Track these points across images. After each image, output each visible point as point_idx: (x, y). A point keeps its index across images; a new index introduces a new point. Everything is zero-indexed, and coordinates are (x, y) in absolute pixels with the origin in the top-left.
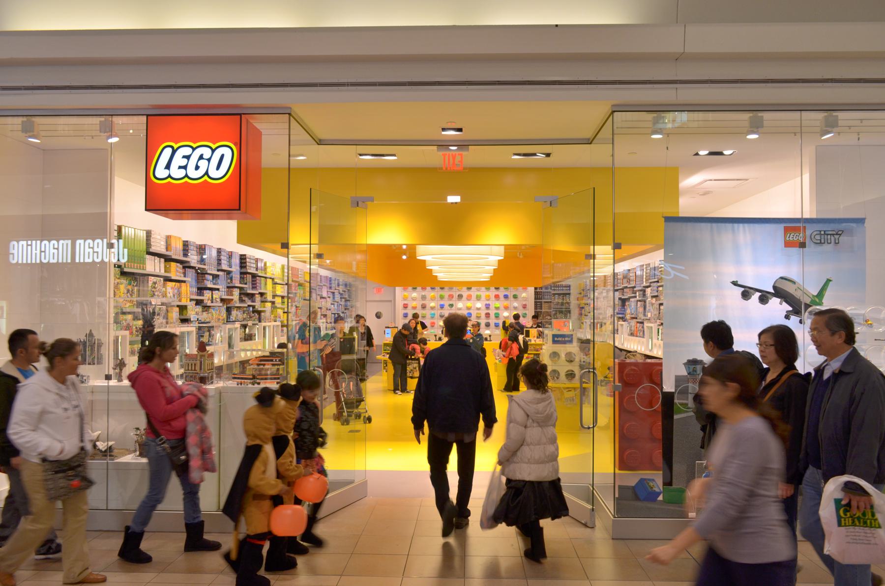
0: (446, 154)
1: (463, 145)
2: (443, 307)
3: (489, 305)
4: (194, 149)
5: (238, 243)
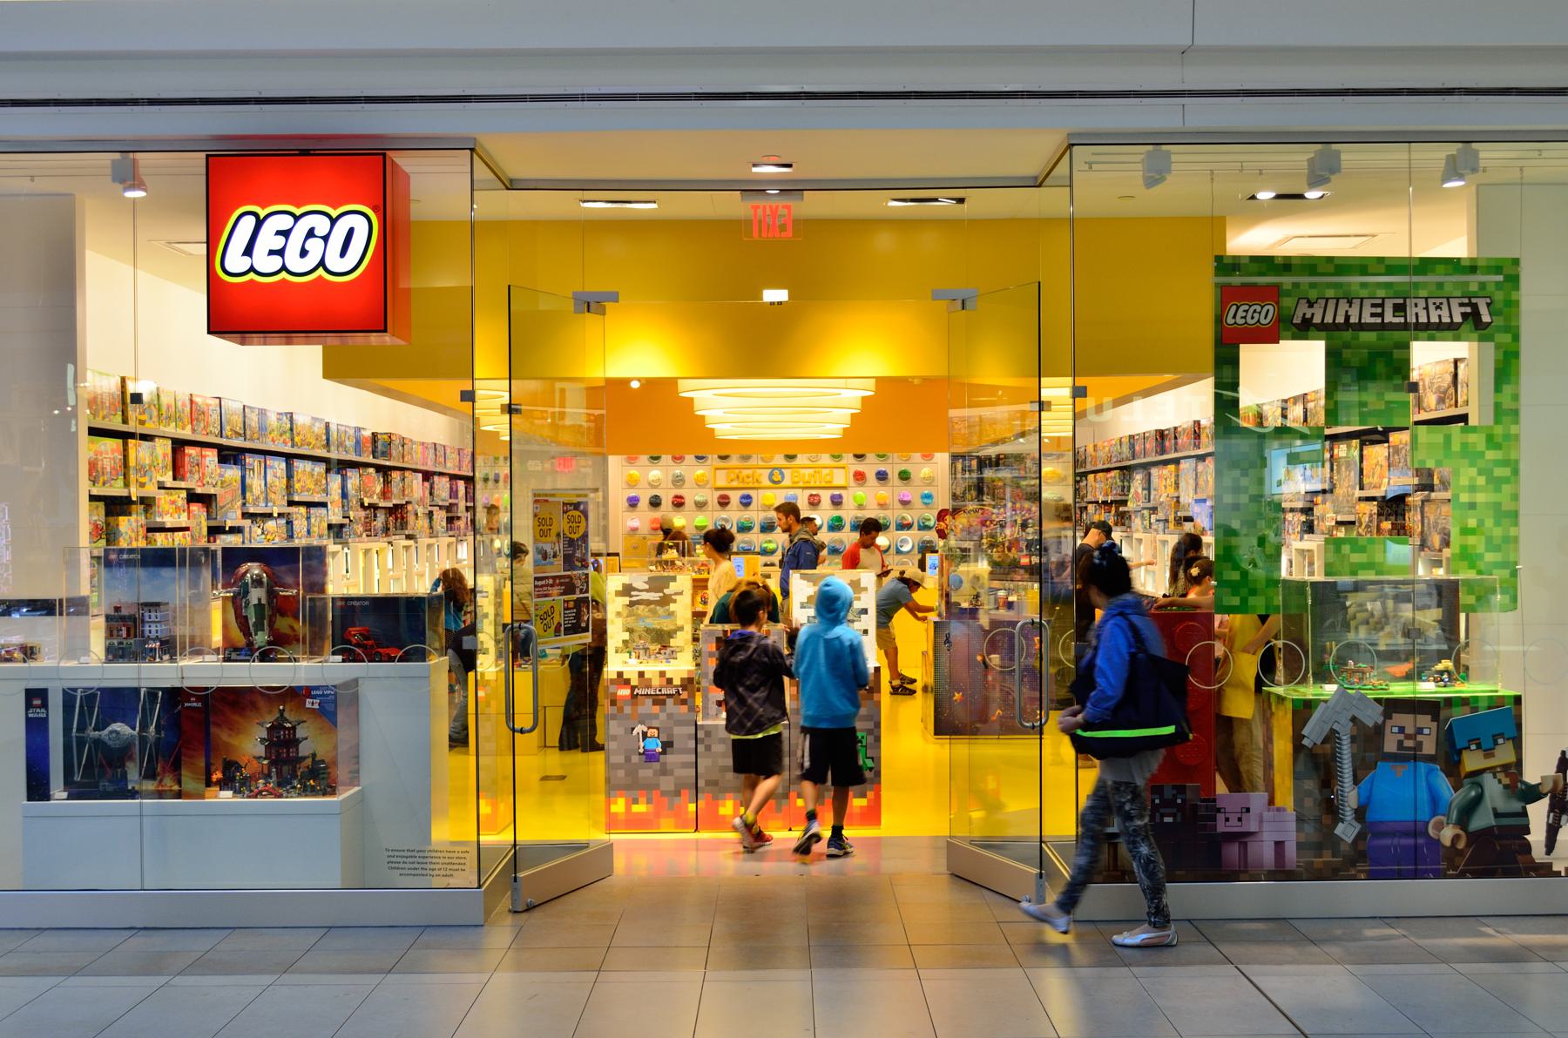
0: (758, 207)
1: (791, 189)
2: (727, 504)
3: (840, 496)
4: (297, 218)
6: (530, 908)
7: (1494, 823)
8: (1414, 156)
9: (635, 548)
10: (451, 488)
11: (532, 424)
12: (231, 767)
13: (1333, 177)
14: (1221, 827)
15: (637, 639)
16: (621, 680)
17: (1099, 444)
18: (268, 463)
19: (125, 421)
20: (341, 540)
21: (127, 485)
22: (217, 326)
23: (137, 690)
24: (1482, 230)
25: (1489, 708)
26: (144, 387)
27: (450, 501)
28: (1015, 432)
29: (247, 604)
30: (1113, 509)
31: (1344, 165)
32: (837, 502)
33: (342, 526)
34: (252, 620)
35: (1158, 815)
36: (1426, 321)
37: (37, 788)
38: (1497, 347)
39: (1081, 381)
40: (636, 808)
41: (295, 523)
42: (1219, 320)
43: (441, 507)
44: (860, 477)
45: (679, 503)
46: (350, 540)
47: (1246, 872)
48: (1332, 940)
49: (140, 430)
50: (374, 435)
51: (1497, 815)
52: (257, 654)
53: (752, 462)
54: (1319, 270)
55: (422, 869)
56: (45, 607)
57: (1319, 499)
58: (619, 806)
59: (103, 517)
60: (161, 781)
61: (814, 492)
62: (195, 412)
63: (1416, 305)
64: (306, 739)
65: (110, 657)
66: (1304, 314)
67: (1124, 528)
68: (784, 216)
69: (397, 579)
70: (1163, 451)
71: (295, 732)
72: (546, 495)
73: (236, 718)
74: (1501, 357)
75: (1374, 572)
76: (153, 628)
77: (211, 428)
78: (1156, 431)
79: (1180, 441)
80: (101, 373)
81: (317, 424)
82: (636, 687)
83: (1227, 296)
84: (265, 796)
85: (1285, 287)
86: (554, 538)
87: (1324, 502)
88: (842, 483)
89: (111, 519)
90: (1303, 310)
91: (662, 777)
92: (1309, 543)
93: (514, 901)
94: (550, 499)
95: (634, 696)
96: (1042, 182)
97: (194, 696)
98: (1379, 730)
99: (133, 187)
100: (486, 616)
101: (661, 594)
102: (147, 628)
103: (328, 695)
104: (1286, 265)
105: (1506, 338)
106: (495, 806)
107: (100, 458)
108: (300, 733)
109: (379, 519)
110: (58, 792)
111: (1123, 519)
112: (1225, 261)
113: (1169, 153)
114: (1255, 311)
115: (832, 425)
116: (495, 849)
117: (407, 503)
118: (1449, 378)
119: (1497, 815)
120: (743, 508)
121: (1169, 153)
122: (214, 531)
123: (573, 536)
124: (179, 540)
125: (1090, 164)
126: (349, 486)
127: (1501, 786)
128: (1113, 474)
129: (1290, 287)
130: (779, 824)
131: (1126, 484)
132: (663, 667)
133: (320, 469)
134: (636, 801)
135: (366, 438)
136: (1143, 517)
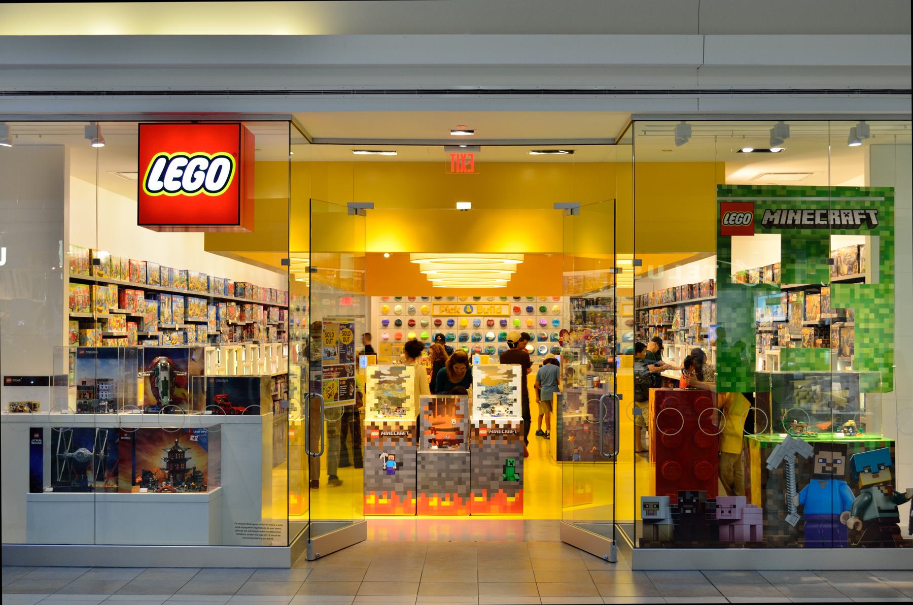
0: (454, 155)
1: (474, 145)
3: (505, 321)
4: (189, 160)
5: (205, 250)
6: (318, 558)
7: (878, 516)
8: (831, 128)
9: (386, 350)
10: (280, 314)
11: (326, 278)
12: (147, 474)
13: (784, 140)
14: (719, 516)
15: (383, 402)
16: (374, 426)
17: (656, 292)
18: (173, 299)
19: (91, 274)
20: (215, 344)
21: (91, 311)
22: (143, 221)
23: (94, 429)
24: (873, 171)
25: (876, 448)
26: (101, 255)
27: (279, 322)
28: (604, 286)
29: (158, 381)
30: (664, 330)
31: (791, 133)
32: (503, 324)
33: (216, 336)
34: (161, 390)
35: (682, 509)
36: (839, 223)
37: (36, 485)
38: (881, 239)
39: (638, 256)
40: (381, 501)
41: (189, 334)
42: (720, 221)
43: (274, 325)
44: (517, 310)
45: (412, 324)
46: (220, 344)
47: (734, 542)
48: (783, 583)
49: (99, 279)
50: (236, 283)
51: (880, 511)
52: (163, 409)
53: (455, 301)
54: (778, 193)
55: (256, 535)
56: (42, 381)
57: (781, 325)
58: (371, 500)
59: (77, 330)
60: (107, 482)
61: (490, 319)
62: (132, 269)
63: (834, 214)
64: (190, 458)
65: (79, 410)
66: (769, 219)
67: (670, 341)
68: (469, 160)
69: (247, 367)
70: (692, 297)
71: (184, 454)
72: (330, 319)
73: (151, 446)
74: (884, 245)
75: (809, 368)
76: (104, 394)
77: (141, 279)
78: (689, 285)
79: (702, 291)
80: (78, 247)
81: (202, 277)
82: (382, 431)
83: (724, 208)
84: (166, 491)
85: (758, 203)
86: (334, 344)
87: (783, 327)
88: (506, 313)
89: (82, 331)
90: (768, 216)
91: (459, 486)
92: (775, 351)
93: (308, 554)
94: (332, 322)
95: (381, 436)
96: (618, 141)
97: (126, 433)
98: (811, 461)
99: (97, 141)
100: (295, 389)
101: (397, 377)
102: (101, 394)
103: (202, 434)
104: (758, 190)
105: (887, 233)
106: (299, 499)
107: (76, 295)
108: (187, 455)
109: (237, 332)
110: (48, 489)
111: (670, 336)
112: (723, 188)
113: (690, 126)
114: (740, 217)
115: (501, 280)
116: (298, 524)
117: (254, 323)
118: (855, 256)
119: (880, 511)
120: (449, 327)
121: (690, 126)
122: (142, 338)
123: (345, 343)
124: (121, 343)
125: (645, 131)
126: (221, 313)
127: (883, 494)
128: (663, 309)
129: (761, 203)
130: (464, 511)
131: (671, 315)
132: (397, 419)
133: (204, 303)
134: (381, 497)
135: (231, 285)
136: (680, 335)
